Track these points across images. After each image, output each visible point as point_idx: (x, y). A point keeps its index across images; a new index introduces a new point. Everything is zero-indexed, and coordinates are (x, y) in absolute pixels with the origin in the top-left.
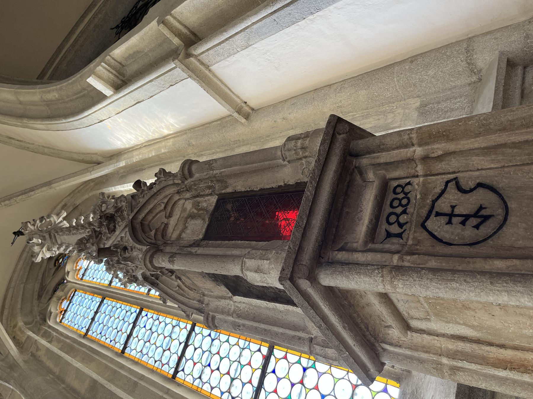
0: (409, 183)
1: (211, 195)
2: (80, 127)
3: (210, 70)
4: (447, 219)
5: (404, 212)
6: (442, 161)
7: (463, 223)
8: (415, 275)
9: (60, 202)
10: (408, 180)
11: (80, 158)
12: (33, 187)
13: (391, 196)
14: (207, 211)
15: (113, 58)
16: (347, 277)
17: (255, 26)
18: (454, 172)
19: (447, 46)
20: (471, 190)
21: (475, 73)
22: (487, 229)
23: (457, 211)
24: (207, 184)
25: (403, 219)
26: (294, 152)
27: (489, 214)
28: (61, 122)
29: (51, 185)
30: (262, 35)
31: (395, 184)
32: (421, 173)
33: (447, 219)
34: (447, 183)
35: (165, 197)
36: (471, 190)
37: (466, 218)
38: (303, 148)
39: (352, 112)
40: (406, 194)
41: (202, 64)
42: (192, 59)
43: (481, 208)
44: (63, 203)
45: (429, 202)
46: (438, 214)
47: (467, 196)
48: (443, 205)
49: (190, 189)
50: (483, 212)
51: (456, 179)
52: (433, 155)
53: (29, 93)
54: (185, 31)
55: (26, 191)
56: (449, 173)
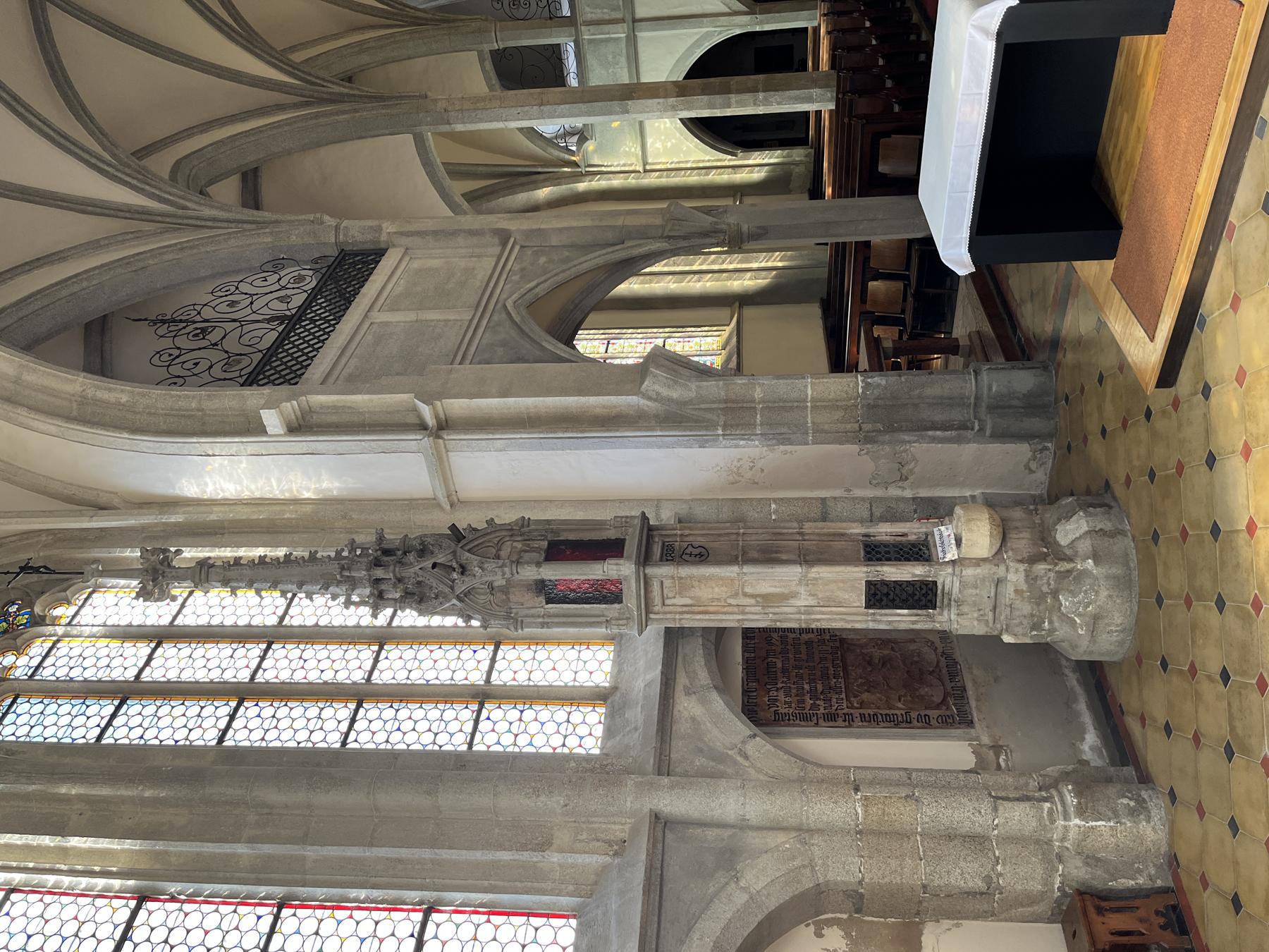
1: (543, 540)
3: (447, 455)
13: (666, 548)
15: (307, 401)
17: (521, 440)
19: (645, 500)
22: (702, 558)
38: (626, 522)
41: (445, 447)
48: (688, 551)
53: (49, 374)
54: (442, 416)
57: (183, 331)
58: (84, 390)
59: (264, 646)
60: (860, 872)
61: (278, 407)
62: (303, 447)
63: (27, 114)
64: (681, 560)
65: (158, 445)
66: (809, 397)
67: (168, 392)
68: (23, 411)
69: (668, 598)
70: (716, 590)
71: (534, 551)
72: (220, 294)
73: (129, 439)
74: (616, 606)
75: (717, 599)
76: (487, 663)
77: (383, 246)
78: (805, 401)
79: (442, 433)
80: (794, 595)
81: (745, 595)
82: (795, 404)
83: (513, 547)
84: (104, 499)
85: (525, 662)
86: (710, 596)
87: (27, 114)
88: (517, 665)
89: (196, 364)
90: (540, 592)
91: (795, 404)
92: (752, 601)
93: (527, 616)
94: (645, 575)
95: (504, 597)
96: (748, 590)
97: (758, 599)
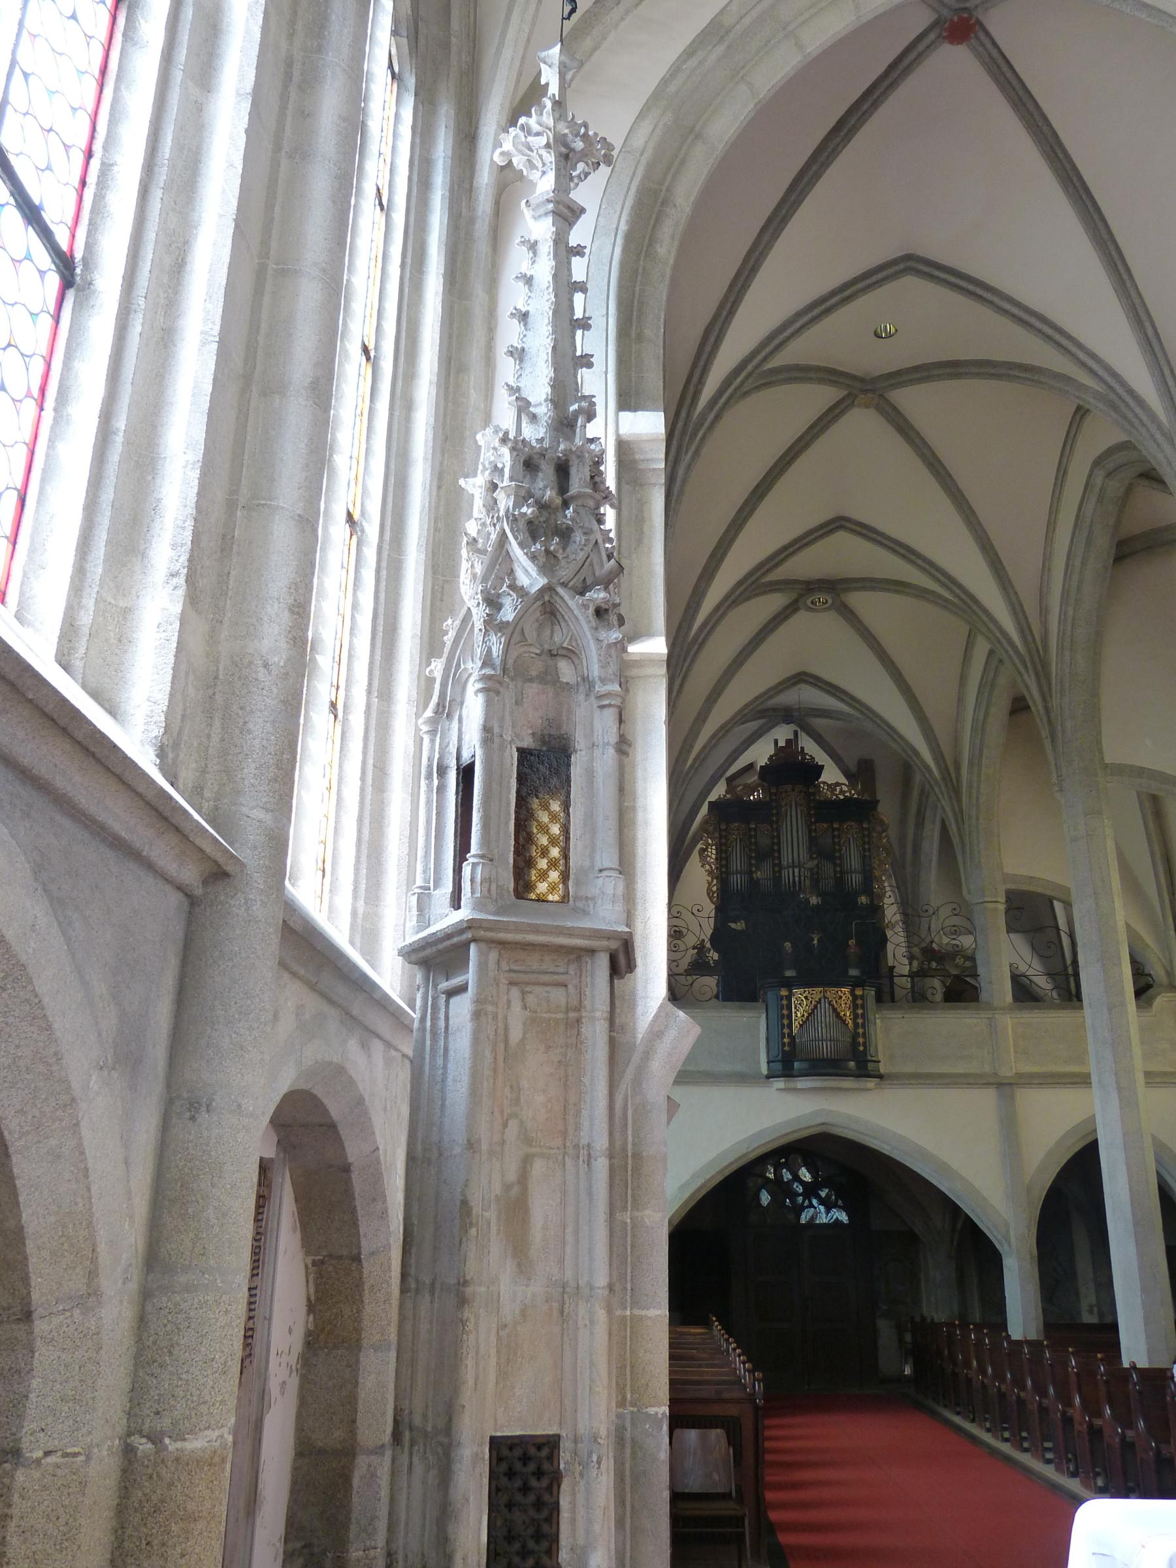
15: (655, 485)
58: (675, 206)
60: (47, 1453)
63: (810, 316)
65: (606, 261)
66: (643, 1313)
69: (523, 993)
70: (540, 1099)
73: (617, 229)
75: (518, 1099)
77: (118, 716)
78: (635, 1304)
80: (524, 1266)
81: (527, 1160)
82: (629, 1286)
86: (525, 1084)
87: (810, 316)
90: (544, 743)
91: (629, 1286)
92: (512, 1176)
94: (592, 952)
95: (534, 673)
96: (538, 1168)
97: (516, 1190)
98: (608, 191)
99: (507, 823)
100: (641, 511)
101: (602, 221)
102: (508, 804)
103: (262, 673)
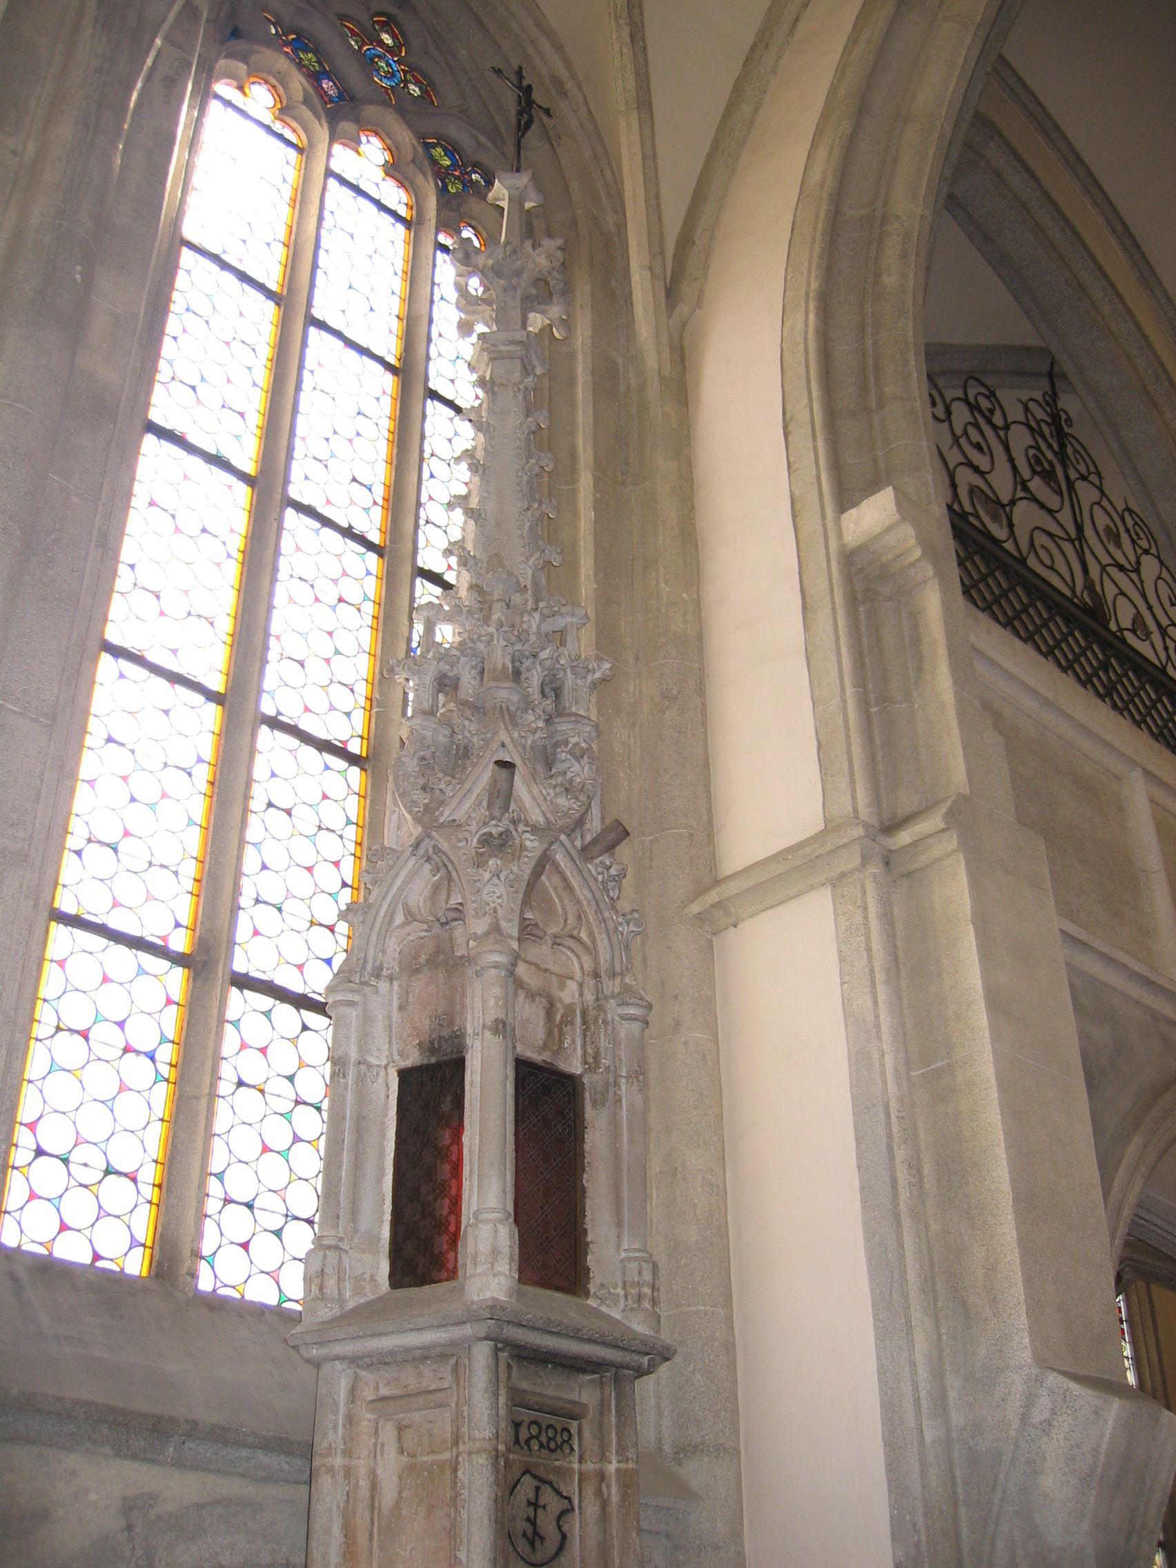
0: (572, 1449)
2: (787, 325)
4: (533, 1500)
5: (541, 1446)
6: (595, 1495)
7: (528, 1519)
8: (492, 1479)
9: (574, 76)
10: (576, 1447)
11: (699, 231)
12: (643, 39)
14: (556, 1053)
16: (486, 1391)
18: (580, 1508)
20: (559, 1527)
21: (678, 1453)
22: (523, 1547)
23: (540, 1511)
24: (603, 1055)
25: (535, 1445)
26: (636, 1279)
27: (537, 1547)
28: (813, 270)
29: (638, 108)
30: (859, 1059)
31: (574, 1430)
32: (584, 1467)
33: (533, 1500)
34: (569, 1499)
35: (591, 934)
36: (559, 1527)
37: (532, 1521)
38: (640, 1297)
39: (657, 1198)
40: (561, 1447)
42: (857, 861)
43: (542, 1538)
44: (569, 85)
45: (551, 1477)
46: (538, 1488)
47: (554, 1523)
48: (547, 1496)
49: (599, 1006)
50: (538, 1541)
51: (573, 1509)
52: (604, 1486)
54: (921, 860)
55: (637, 10)
56: (580, 1502)
57: (1043, 445)
59: (375, 537)
61: (904, 519)
62: (819, 586)
64: (516, 1471)
65: (800, 340)
67: (912, 346)
68: (846, 127)
71: (550, 1032)
72: (1130, 523)
74: (384, 1268)
76: (297, 987)
79: (875, 869)
83: (564, 978)
84: (687, 290)
85: (291, 1078)
88: (283, 1057)
89: (978, 447)
93: (367, 1018)
98: (792, 255)
99: (379, 1180)
100: (915, 627)
101: (790, 294)
102: (382, 1155)
103: (558, 1005)
